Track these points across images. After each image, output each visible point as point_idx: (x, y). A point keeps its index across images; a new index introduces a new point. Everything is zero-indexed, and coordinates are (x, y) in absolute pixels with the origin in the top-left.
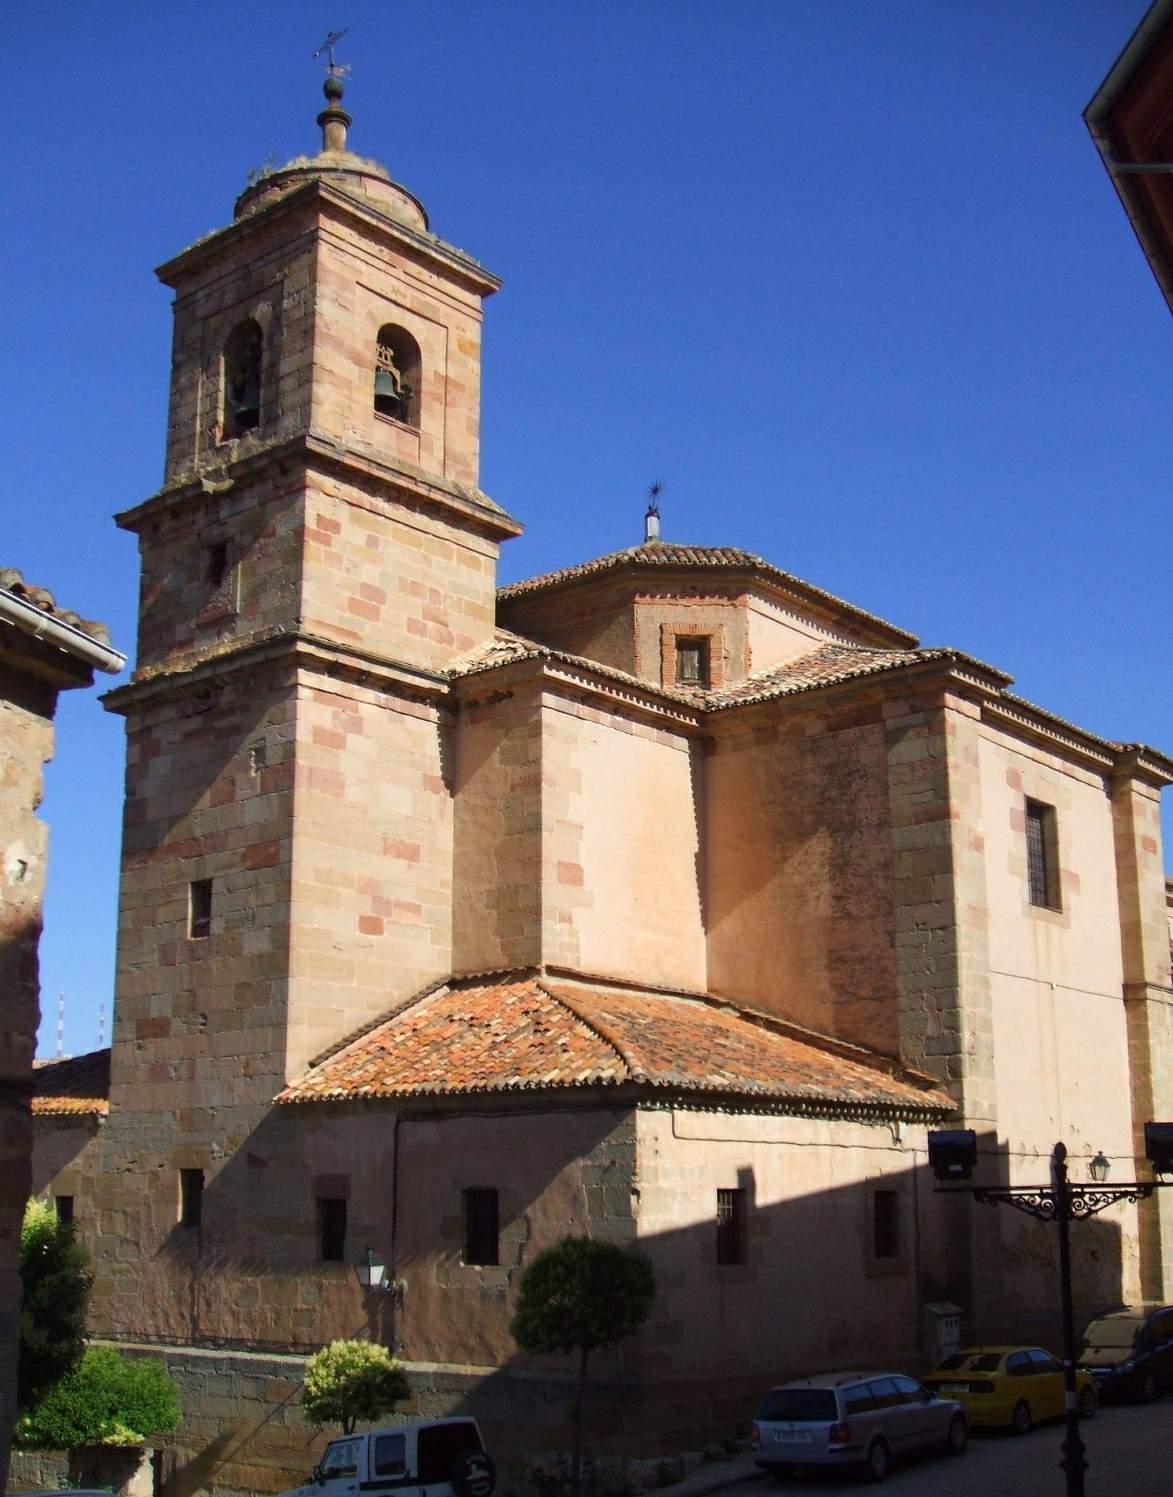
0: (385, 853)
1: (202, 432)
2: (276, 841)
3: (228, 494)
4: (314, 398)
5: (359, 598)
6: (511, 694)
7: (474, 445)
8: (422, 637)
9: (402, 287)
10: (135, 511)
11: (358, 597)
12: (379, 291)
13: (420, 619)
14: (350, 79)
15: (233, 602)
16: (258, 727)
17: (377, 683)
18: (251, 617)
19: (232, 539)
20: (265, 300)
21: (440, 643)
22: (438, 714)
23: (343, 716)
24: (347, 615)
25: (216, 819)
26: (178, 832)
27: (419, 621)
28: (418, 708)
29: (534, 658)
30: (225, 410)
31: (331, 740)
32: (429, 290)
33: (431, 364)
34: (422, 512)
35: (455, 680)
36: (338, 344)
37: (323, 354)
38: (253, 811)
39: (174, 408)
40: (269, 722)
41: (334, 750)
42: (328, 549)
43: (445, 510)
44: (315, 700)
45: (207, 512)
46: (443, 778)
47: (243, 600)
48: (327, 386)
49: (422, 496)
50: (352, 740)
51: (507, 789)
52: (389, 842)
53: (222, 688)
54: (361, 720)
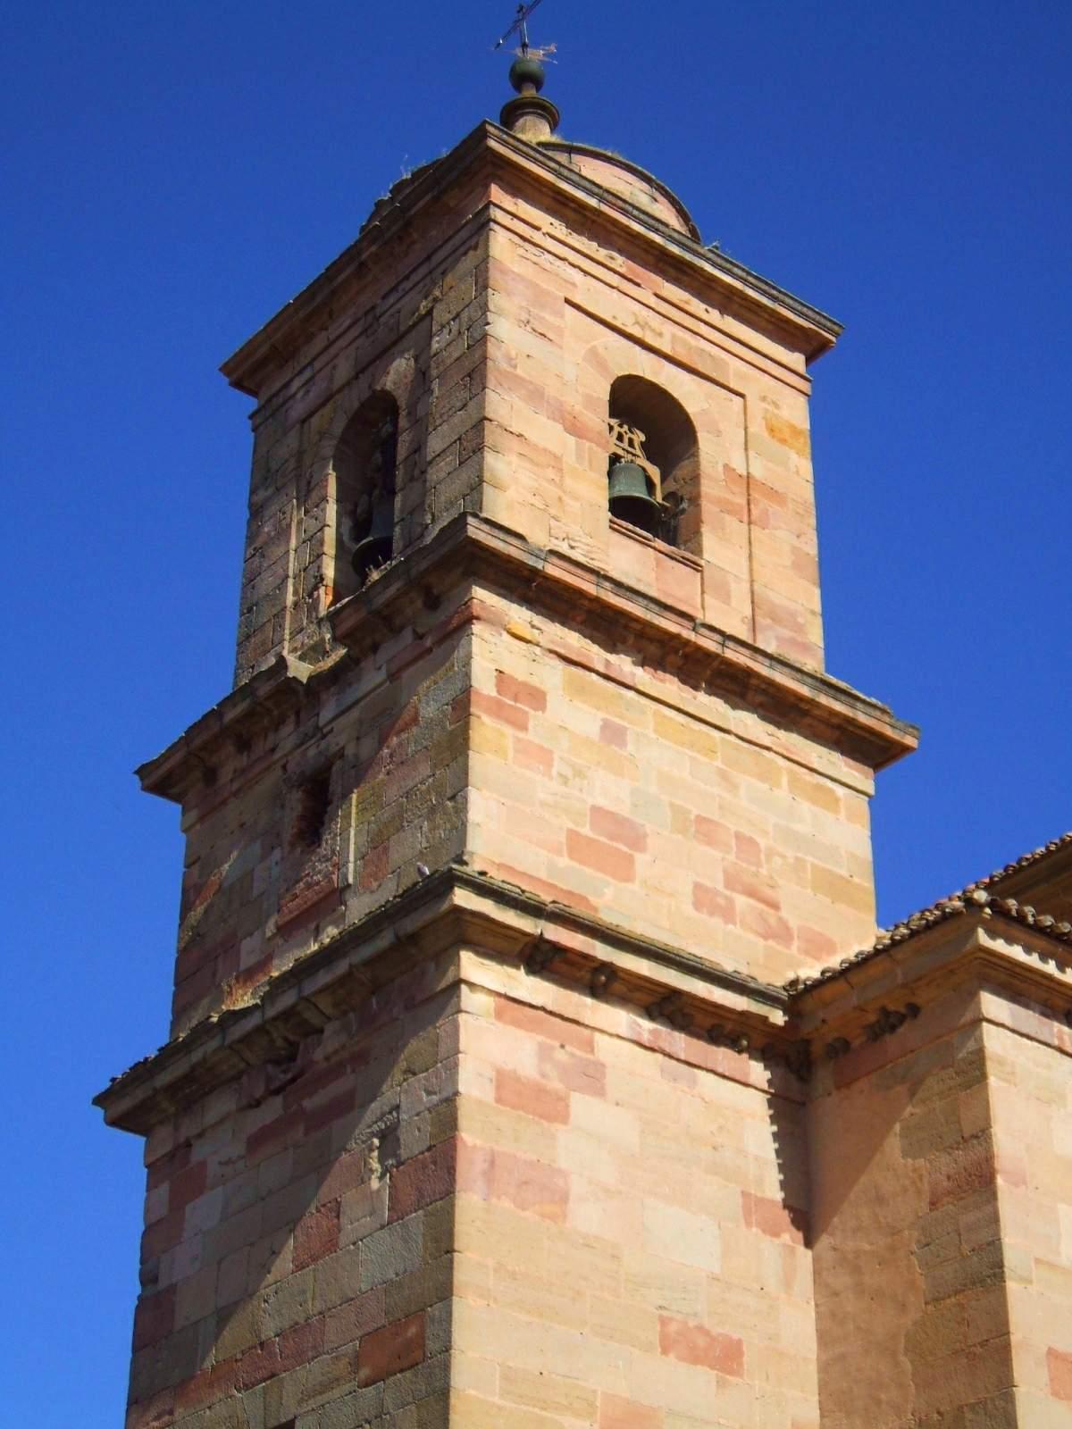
0: (665, 1351)
1: (296, 604)
2: (418, 1314)
3: (336, 677)
4: (487, 476)
5: (591, 834)
6: (914, 1010)
7: (810, 598)
8: (726, 923)
9: (655, 321)
10: (172, 749)
11: (586, 830)
12: (609, 319)
13: (720, 887)
14: (555, 62)
15: (340, 866)
16: (385, 1088)
17: (637, 995)
18: (375, 885)
19: (341, 754)
20: (401, 354)
21: (766, 938)
22: (768, 1075)
23: (560, 1055)
24: (564, 861)
25: (304, 1292)
26: (234, 1335)
27: (717, 893)
28: (723, 1057)
29: (956, 914)
30: (338, 558)
31: (536, 1102)
32: (703, 329)
33: (718, 451)
34: (712, 691)
35: (798, 998)
36: (536, 395)
37: (501, 404)
38: (372, 1257)
39: (250, 580)
40: (405, 1072)
41: (545, 1124)
42: (521, 735)
43: (758, 690)
44: (499, 1015)
45: (298, 723)
46: (787, 1205)
47: (361, 857)
48: (514, 459)
49: (709, 655)
50: (580, 1104)
51: (924, 1206)
52: (673, 1327)
53: (321, 1031)
54: (601, 1066)
